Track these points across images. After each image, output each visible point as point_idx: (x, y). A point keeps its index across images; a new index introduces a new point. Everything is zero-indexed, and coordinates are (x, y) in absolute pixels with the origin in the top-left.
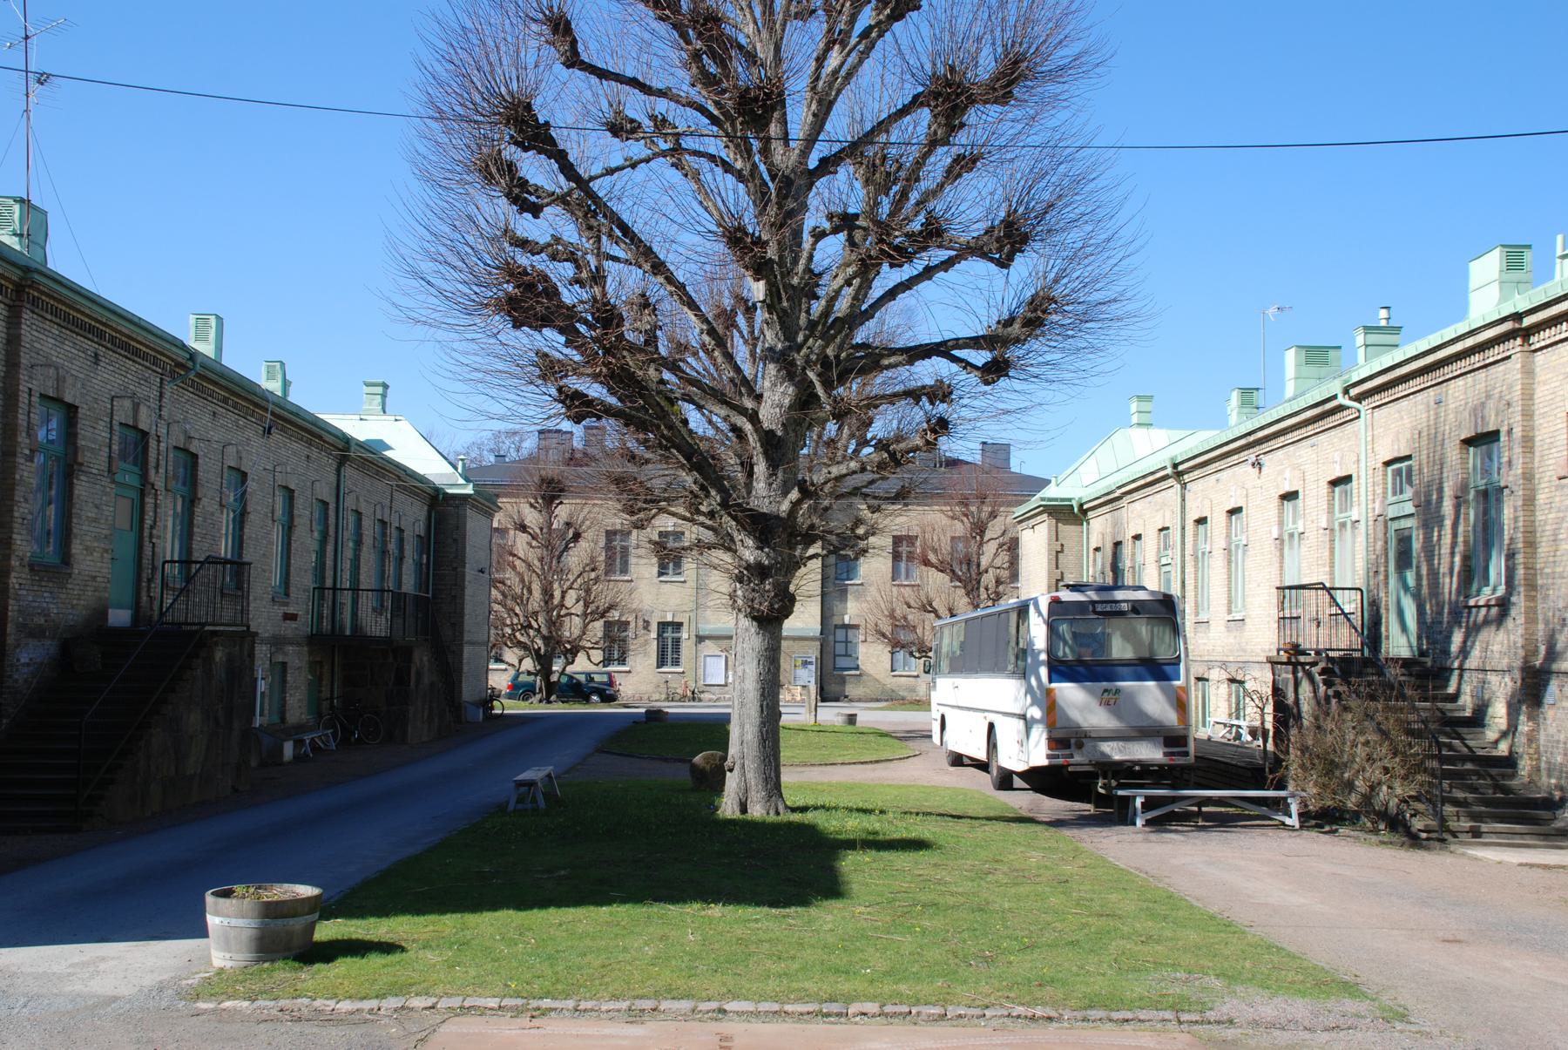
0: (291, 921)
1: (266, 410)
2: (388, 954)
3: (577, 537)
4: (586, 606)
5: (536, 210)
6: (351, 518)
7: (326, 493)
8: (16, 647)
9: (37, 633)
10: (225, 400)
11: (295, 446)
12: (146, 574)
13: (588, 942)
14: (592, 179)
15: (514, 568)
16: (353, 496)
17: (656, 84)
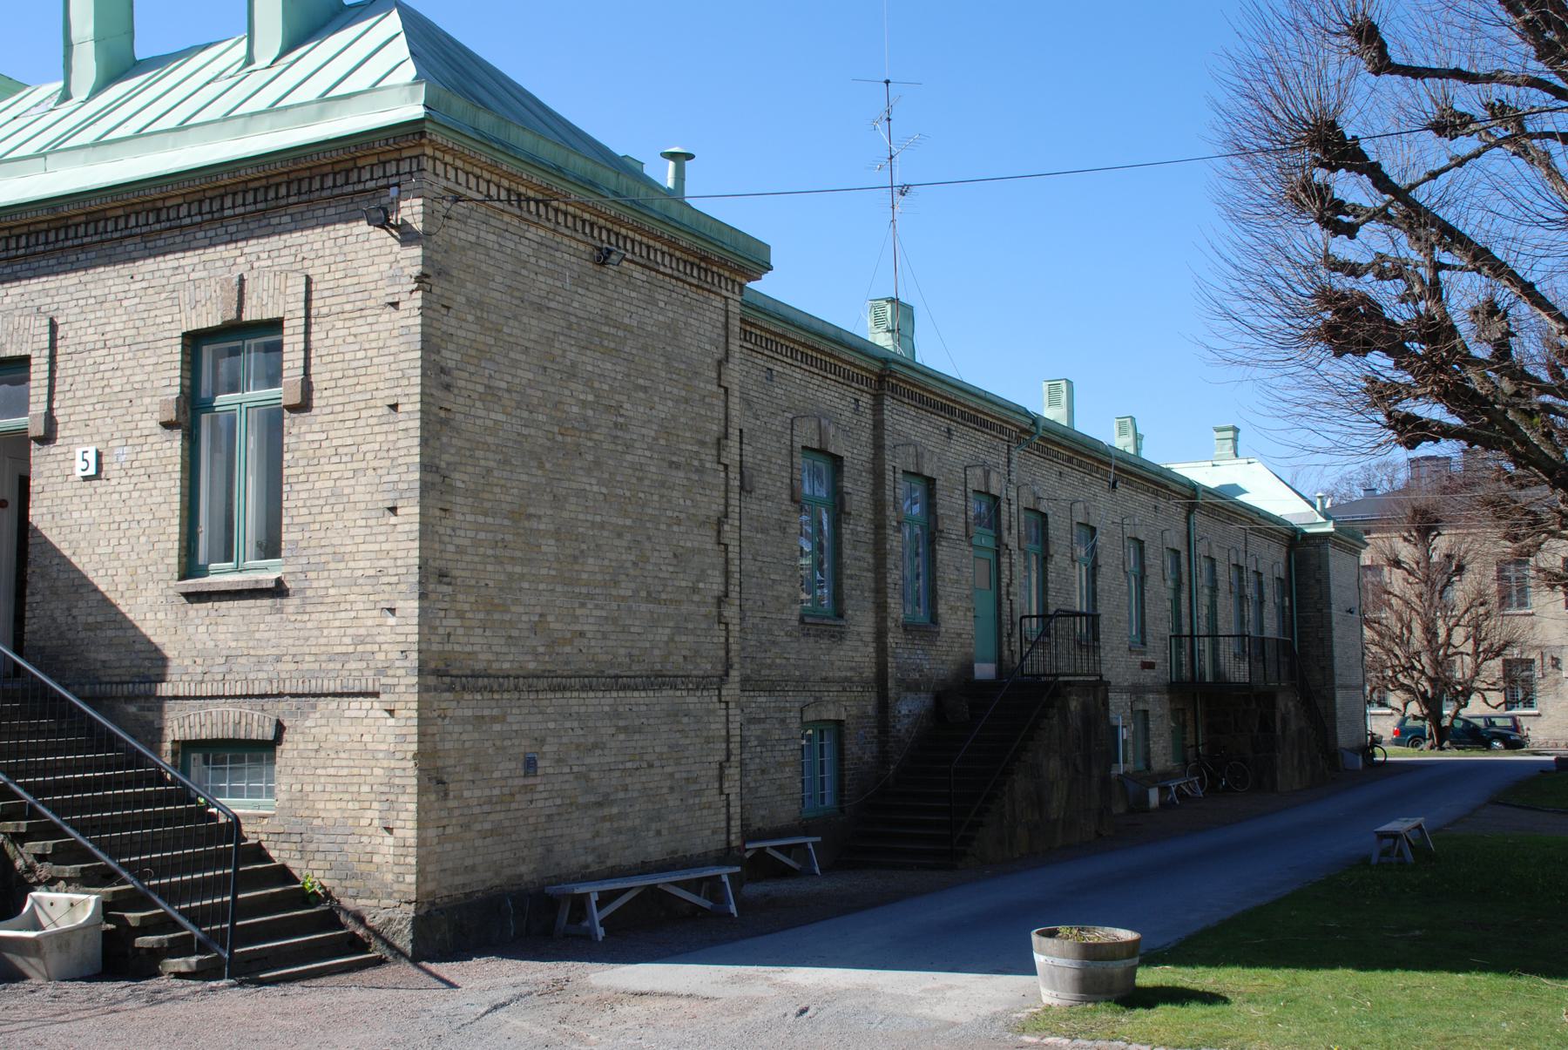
0: (1111, 964)
1: (1109, 465)
2: (1210, 1004)
3: (1460, 569)
4: (1477, 643)
5: (1351, 231)
6: (1205, 565)
7: (1177, 542)
8: (897, 700)
9: (913, 687)
10: (1070, 460)
11: (1142, 497)
12: (1006, 628)
13: (1433, 1011)
14: (1412, 187)
15: (1390, 606)
16: (1205, 542)
17: (1482, 68)
